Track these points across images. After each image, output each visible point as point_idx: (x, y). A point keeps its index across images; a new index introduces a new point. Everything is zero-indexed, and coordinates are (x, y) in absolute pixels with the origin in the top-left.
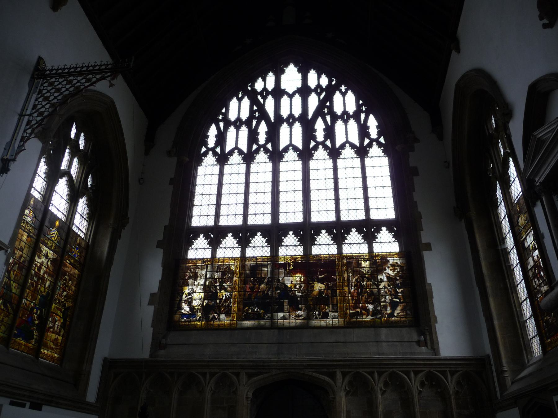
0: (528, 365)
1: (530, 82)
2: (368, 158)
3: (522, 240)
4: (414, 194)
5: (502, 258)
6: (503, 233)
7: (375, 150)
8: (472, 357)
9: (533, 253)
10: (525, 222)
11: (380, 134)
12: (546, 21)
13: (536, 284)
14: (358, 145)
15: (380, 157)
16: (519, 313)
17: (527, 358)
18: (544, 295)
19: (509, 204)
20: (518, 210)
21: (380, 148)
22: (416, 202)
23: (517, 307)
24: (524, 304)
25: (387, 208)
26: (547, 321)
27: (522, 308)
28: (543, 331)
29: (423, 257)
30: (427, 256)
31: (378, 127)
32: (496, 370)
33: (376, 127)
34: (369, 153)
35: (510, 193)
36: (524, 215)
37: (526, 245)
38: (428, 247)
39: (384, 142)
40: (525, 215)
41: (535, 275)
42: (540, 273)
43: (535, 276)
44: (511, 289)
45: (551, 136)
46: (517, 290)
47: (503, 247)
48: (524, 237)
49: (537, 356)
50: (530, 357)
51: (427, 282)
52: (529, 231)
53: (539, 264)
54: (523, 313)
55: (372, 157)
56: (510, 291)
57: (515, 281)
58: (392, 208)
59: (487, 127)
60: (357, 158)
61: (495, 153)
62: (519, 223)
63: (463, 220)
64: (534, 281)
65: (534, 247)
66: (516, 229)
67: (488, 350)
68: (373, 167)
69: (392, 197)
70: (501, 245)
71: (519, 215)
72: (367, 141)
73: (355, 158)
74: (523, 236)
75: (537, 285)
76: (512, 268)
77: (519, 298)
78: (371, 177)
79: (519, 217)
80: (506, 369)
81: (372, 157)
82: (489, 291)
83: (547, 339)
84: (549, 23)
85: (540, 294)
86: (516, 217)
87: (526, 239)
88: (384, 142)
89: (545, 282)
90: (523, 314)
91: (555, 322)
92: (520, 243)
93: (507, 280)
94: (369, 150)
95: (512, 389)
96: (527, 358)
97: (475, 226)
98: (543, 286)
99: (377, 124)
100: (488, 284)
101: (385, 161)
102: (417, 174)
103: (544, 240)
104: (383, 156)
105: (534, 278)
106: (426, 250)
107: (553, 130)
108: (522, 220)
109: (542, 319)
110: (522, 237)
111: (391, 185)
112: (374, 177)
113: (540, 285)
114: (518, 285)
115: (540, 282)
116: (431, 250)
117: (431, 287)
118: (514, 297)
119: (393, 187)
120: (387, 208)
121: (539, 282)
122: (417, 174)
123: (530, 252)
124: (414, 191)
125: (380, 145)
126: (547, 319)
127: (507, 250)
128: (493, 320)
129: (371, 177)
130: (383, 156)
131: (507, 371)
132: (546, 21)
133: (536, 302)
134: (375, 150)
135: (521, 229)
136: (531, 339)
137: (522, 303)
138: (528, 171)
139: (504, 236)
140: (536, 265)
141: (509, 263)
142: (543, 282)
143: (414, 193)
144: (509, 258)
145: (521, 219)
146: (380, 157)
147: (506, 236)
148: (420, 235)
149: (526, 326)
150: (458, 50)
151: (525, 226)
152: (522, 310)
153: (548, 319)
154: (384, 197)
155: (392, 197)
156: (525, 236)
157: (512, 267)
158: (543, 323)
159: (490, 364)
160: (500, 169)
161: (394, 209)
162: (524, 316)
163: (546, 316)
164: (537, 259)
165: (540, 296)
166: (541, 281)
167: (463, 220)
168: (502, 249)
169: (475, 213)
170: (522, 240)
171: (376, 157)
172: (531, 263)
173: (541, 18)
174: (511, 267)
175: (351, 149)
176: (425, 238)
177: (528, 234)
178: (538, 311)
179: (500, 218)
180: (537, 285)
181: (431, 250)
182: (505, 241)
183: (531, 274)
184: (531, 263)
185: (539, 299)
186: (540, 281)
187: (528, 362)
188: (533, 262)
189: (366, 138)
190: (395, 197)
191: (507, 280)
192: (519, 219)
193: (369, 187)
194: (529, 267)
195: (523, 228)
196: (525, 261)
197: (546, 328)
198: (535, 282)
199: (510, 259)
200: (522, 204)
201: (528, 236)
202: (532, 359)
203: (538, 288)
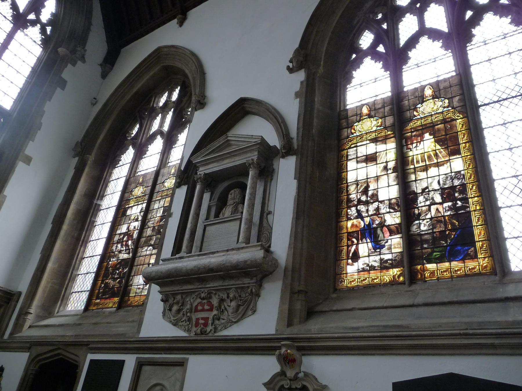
0: (55, 314)
1: (243, 96)
2: (22, 33)
3: (127, 206)
4: (48, 103)
5: (92, 211)
6: (106, 191)
7: (34, 32)
8: (2, 288)
9: (131, 222)
10: (141, 194)
11: (50, 22)
12: (291, 65)
13: (116, 249)
14: (21, 11)
15: (35, 42)
16: (76, 266)
17: (59, 308)
18: (119, 261)
19: (133, 172)
20: (140, 181)
21: (40, 35)
22: (44, 112)
23: (78, 260)
24: (86, 260)
25: (7, 95)
26: (107, 285)
27: (82, 262)
28: (97, 291)
29: (17, 167)
30: (20, 167)
31: (53, 15)
32: (21, 309)
33: (51, 13)
34: (27, 29)
35: (139, 163)
36: (144, 188)
37: (129, 212)
38: (28, 160)
39: (48, 33)
40: (145, 189)
41: (121, 241)
42: (127, 241)
43: (120, 241)
44: (83, 242)
45: (245, 145)
46: (88, 245)
47: (99, 202)
48: (130, 205)
49: (69, 310)
50: (62, 308)
51: (3, 192)
52: (140, 203)
53: (131, 234)
54: (80, 267)
55: (27, 35)
56: (81, 242)
57: (90, 236)
58: (13, 99)
59: (155, 100)
60: (10, 21)
61: (148, 124)
62: (133, 191)
63: (77, 159)
64: (116, 245)
65: (136, 217)
66: (126, 195)
67: (23, 286)
68: (21, 45)
69: (20, 88)
70: (98, 199)
71: (139, 185)
72: (32, 17)
73: (8, 20)
74: (131, 204)
75: (117, 250)
76: (95, 225)
77: (85, 253)
78: (12, 52)
79: (137, 187)
80: (32, 312)
81: (27, 35)
82: (62, 233)
83: (96, 299)
84: (292, 68)
85: (116, 259)
86: (133, 185)
87: (132, 208)
88: (48, 33)
89: (128, 251)
90: (80, 268)
91: (116, 288)
92: (123, 208)
93: (84, 233)
94: (28, 26)
95: (26, 332)
96: (59, 308)
97: (86, 170)
98: (124, 254)
99: (54, 11)
100: (65, 227)
101: (38, 51)
102: (63, 88)
103: (169, 219)
104: (38, 44)
105: (118, 243)
106: (24, 162)
107: (249, 143)
108: (138, 191)
109: (103, 281)
110: (129, 205)
111: (27, 77)
112: (15, 55)
113: (120, 252)
114: (91, 241)
115: (122, 249)
116: (29, 165)
117: (5, 200)
118: (81, 250)
119: (28, 80)
120: (7, 95)
121: (121, 248)
122: (63, 88)
123: (129, 220)
124: (50, 100)
125: (43, 31)
126: (109, 282)
127: (101, 207)
128: (49, 261)
129: (12, 52)
130: (38, 44)
131: (31, 314)
132: (291, 65)
133: (105, 264)
134: (34, 32)
135: (132, 198)
136: (73, 292)
137: (85, 258)
138: (199, 158)
139: (105, 194)
140: (129, 234)
141: (95, 218)
142: (126, 250)
143: (48, 102)
144: (98, 214)
145: (138, 189)
146: (35, 42)
147: (106, 195)
148: (27, 145)
149: (76, 279)
150: (181, 23)
151: (138, 197)
152: (81, 264)
153: (110, 283)
154: (12, 82)
155: (20, 88)
156: (132, 205)
157: (95, 223)
158: (102, 283)
159: (17, 302)
160: (144, 139)
161: (14, 100)
162: (79, 270)
163: (110, 279)
164: (133, 229)
165: (114, 260)
166: (124, 249)
167: (77, 159)
168: (96, 204)
169: (93, 159)
170: (127, 206)
171: (31, 39)
172: (124, 229)
173: (291, 61)
174: (94, 223)
175: (11, 8)
176: (30, 149)
177: (138, 205)
178: (103, 272)
179: (111, 177)
180: (117, 250)
181: (29, 165)
182: (103, 199)
183: (116, 238)
184: (124, 229)
185: (110, 263)
186: (123, 248)
187: (58, 313)
188: (127, 230)
189: (33, 13)
190: (22, 90)
191: (84, 233)
192: (135, 188)
193: (3, 60)
194: (119, 232)
195: (135, 198)
196: (118, 225)
197: (102, 289)
198: (117, 246)
199: (98, 216)
200: (148, 178)
201: (136, 207)
202: (63, 310)
203: (117, 253)
